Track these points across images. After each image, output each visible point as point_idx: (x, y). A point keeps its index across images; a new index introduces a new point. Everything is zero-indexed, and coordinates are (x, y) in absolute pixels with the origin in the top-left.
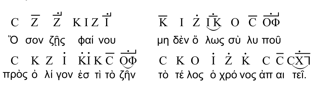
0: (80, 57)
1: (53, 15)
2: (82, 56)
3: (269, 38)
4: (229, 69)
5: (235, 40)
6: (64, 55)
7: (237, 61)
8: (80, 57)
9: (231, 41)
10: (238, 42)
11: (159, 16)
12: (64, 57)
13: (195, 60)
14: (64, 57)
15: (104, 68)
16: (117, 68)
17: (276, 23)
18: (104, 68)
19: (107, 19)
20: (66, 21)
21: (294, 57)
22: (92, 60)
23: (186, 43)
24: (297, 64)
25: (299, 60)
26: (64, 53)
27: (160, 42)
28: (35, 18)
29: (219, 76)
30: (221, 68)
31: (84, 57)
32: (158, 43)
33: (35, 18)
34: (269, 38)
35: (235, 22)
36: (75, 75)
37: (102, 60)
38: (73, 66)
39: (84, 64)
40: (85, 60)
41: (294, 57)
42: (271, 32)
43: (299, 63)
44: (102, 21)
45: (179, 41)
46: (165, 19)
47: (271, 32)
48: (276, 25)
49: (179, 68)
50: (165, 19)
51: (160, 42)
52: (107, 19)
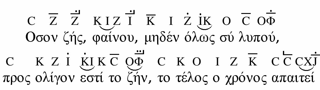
0: (83, 58)
1: (49, 14)
2: (85, 56)
3: (260, 36)
4: (235, 71)
5: (227, 37)
6: (68, 56)
7: (243, 61)
8: (83, 58)
9: (223, 38)
10: (231, 39)
11: (147, 15)
12: (68, 58)
13: (197, 61)
14: (68, 58)
15: (107, 71)
16: (121, 69)
17: (271, 21)
18: (107, 71)
19: (130, 18)
20: (86, 20)
21: (302, 58)
22: (96, 62)
23: (176, 41)
24: (305, 65)
25: (308, 61)
26: (68, 54)
27: (148, 39)
28: (53, 18)
29: (224, 80)
30: (225, 70)
31: (87, 58)
32: (146, 41)
33: (53, 18)
34: (260, 36)
35: (226, 21)
36: (77, 79)
37: (106, 61)
38: (75, 69)
39: (87, 65)
40: (88, 61)
41: (302, 58)
42: (266, 30)
43: (308, 64)
44: (124, 20)
45: (167, 38)
46: (153, 17)
47: (266, 30)
48: (271, 24)
49: (180, 70)
50: (153, 17)
51: (148, 39)
52: (130, 18)
